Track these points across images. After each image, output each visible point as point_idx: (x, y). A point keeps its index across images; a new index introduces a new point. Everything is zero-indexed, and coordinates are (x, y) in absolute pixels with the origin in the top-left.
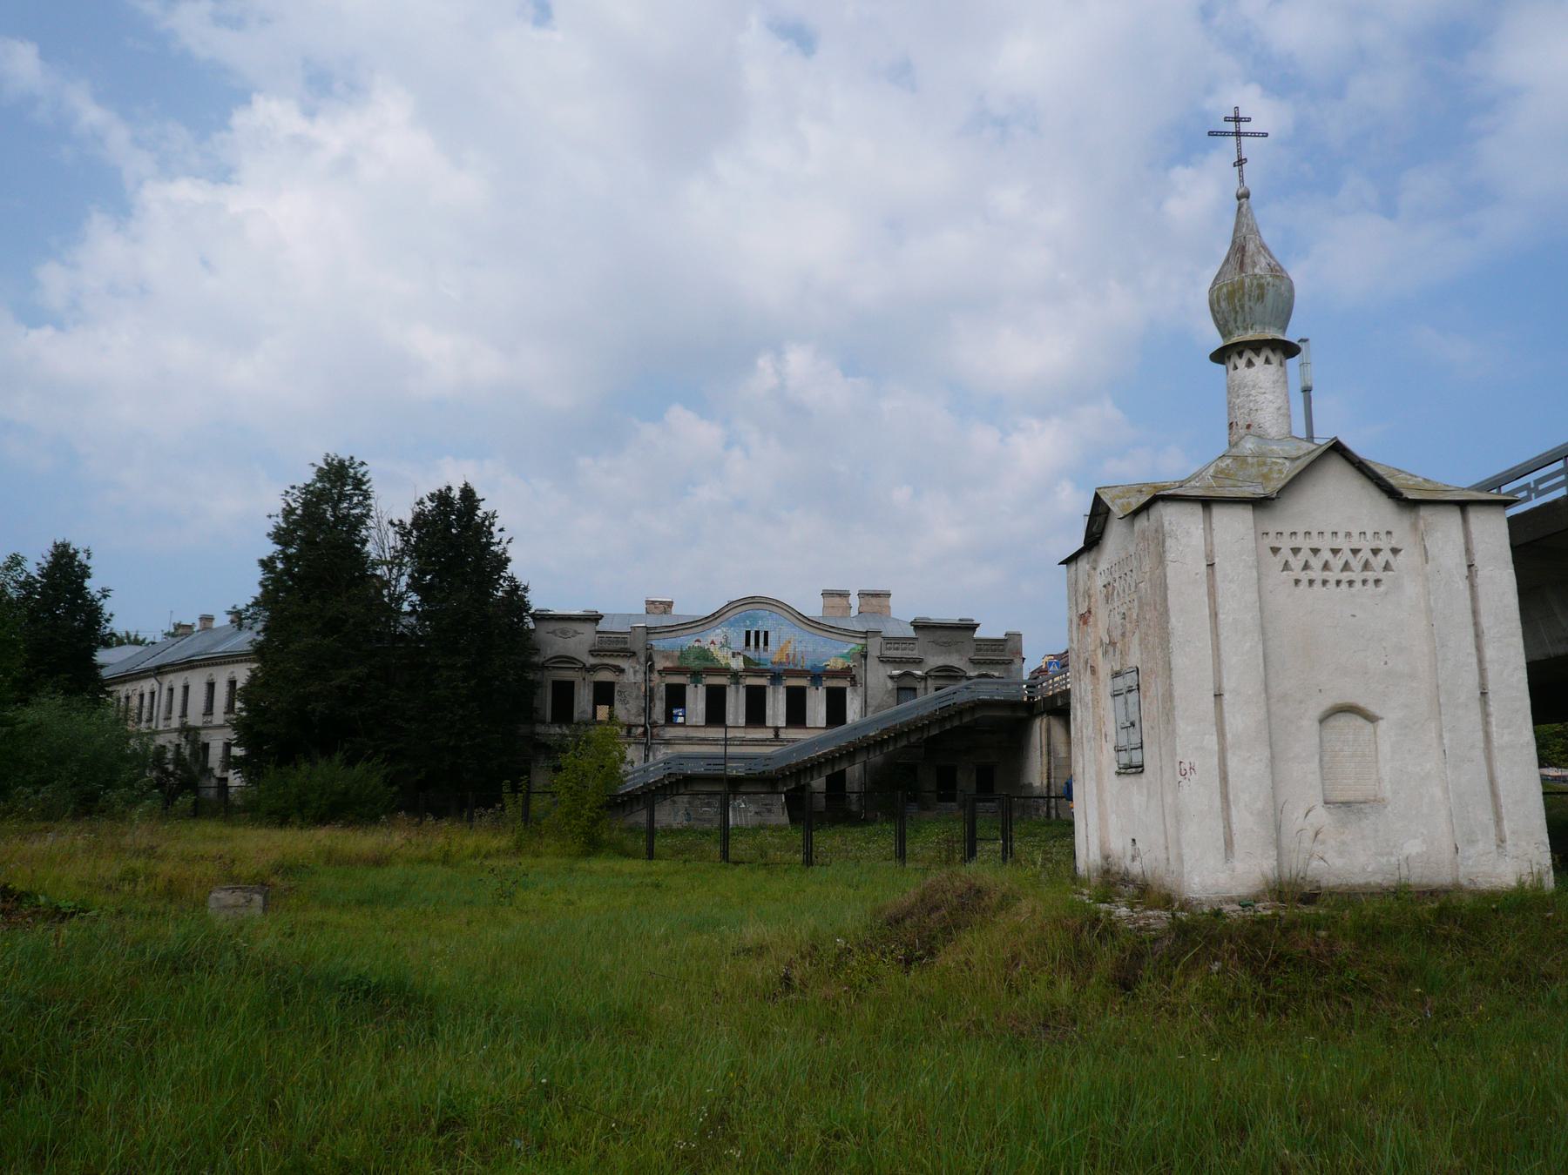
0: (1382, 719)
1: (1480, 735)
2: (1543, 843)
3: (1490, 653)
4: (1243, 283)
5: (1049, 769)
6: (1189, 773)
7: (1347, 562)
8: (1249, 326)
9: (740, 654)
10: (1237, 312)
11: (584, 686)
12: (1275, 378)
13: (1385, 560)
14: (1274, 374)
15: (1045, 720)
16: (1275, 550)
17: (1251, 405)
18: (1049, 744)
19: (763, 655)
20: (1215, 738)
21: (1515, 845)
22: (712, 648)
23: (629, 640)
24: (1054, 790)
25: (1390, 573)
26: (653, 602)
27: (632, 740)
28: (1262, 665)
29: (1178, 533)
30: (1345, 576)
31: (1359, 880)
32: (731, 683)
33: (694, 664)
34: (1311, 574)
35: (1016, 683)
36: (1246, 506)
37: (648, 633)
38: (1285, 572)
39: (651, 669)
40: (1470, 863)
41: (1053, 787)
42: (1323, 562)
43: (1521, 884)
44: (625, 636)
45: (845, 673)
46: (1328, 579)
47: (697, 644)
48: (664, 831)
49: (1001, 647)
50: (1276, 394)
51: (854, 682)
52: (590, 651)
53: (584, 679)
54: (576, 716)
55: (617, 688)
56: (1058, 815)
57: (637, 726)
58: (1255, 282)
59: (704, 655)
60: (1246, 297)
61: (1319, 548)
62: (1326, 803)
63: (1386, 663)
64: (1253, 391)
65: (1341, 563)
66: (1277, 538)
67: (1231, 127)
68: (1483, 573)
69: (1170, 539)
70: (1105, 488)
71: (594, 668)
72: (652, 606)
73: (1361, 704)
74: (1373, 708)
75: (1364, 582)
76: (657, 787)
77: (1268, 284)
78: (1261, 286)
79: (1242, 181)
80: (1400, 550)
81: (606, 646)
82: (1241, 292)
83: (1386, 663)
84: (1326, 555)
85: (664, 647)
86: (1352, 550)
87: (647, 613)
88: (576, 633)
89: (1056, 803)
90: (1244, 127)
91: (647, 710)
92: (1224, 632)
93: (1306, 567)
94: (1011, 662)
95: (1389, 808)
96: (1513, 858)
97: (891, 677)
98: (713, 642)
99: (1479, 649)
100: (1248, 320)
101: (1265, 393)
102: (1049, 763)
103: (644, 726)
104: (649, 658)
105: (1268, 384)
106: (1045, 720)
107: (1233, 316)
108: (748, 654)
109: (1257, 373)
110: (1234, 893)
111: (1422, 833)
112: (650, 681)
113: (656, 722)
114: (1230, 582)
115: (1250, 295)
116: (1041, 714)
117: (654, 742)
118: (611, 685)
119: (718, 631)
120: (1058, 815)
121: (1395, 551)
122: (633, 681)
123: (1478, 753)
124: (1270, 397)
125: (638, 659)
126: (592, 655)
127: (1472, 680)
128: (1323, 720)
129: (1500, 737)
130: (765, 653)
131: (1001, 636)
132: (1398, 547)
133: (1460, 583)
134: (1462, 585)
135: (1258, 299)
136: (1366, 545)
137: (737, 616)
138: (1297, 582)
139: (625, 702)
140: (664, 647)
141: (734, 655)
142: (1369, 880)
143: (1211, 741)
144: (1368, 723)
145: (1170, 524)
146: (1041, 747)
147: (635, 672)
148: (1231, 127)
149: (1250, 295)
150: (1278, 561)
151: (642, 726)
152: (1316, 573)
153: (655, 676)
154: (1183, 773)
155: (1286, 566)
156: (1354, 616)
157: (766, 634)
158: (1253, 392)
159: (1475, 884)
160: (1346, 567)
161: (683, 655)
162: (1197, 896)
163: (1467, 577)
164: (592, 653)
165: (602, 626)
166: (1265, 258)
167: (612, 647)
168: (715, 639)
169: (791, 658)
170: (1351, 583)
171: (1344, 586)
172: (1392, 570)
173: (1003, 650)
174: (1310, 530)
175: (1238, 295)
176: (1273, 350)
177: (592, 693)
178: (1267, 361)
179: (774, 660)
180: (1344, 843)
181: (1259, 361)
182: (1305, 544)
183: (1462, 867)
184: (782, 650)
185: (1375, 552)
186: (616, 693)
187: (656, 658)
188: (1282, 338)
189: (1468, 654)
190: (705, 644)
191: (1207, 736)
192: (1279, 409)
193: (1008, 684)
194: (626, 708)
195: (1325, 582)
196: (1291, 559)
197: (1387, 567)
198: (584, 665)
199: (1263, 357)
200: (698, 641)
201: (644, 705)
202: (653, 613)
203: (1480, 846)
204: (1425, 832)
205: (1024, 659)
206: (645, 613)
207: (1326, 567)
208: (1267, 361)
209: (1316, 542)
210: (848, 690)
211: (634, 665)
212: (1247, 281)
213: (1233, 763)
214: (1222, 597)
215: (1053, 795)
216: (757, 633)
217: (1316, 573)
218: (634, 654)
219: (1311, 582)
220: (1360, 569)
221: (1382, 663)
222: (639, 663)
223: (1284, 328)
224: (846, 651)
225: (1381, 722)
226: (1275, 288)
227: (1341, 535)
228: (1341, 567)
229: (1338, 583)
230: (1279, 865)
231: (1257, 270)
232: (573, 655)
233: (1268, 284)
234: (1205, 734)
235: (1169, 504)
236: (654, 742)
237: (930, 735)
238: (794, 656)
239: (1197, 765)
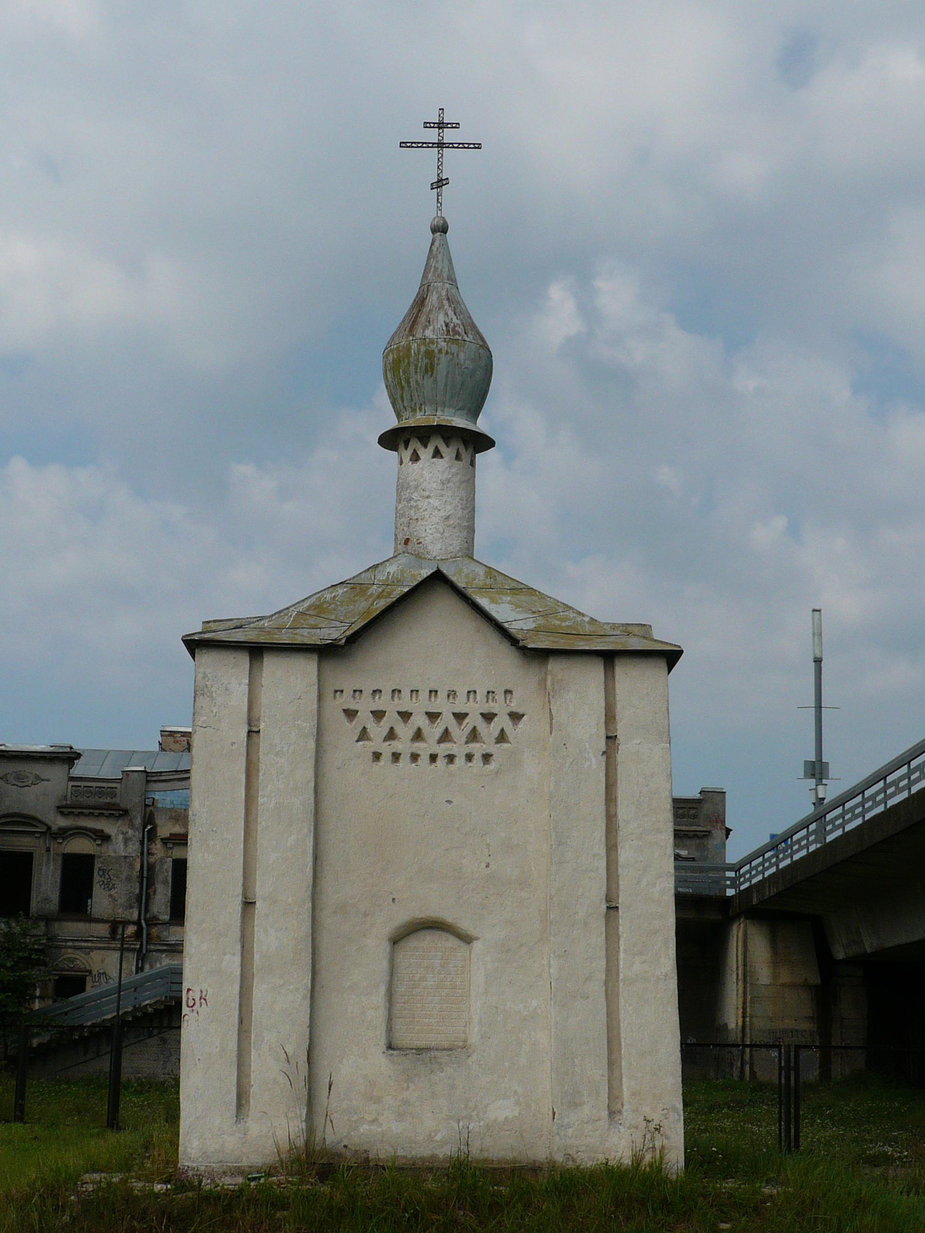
0: (477, 939)
1: (601, 963)
2: (675, 1109)
3: (625, 855)
4: (409, 349)
5: (744, 1003)
6: (198, 1004)
7: (446, 730)
8: (418, 406)
10: (402, 388)
11: (48, 860)
12: (446, 476)
13: (500, 728)
14: (444, 472)
15: (742, 925)
16: (351, 714)
17: (412, 512)
18: (745, 965)
20: (238, 959)
21: (636, 1111)
23: (118, 791)
24: (749, 1035)
25: (505, 745)
26: (172, 733)
28: (310, 864)
29: (214, 689)
31: (423, 1151)
34: (397, 746)
35: (716, 869)
36: (309, 655)
37: (148, 782)
38: (361, 743)
39: (152, 835)
40: (570, 1131)
41: (748, 1030)
42: (415, 729)
43: (637, 1160)
44: (114, 785)
46: (418, 752)
48: (141, 1084)
49: (692, 812)
50: (444, 499)
52: (58, 807)
53: (48, 850)
54: (34, 905)
55: (97, 865)
56: (753, 1073)
58: (423, 349)
60: (412, 368)
61: (410, 711)
62: (390, 1047)
63: (487, 866)
64: (416, 494)
65: (438, 731)
66: (354, 697)
67: (432, 135)
69: (202, 697)
70: (215, 621)
71: (64, 834)
72: (171, 739)
73: (448, 917)
74: (465, 925)
75: (469, 757)
76: (134, 1017)
77: (440, 351)
78: (429, 354)
79: (439, 209)
80: (523, 715)
81: (83, 800)
82: (406, 361)
83: (487, 866)
85: (172, 802)
86: (454, 714)
87: (163, 750)
88: (39, 779)
89: (751, 1056)
90: (449, 136)
91: (143, 899)
92: (263, 821)
93: (391, 735)
94: (707, 835)
95: (474, 1057)
96: (629, 1128)
99: (611, 848)
100: (415, 398)
101: (428, 497)
102: (745, 993)
104: (149, 819)
105: (434, 485)
106: (742, 925)
107: (399, 392)
109: (422, 469)
110: (245, 1163)
111: (515, 1091)
112: (149, 854)
113: (155, 918)
114: (277, 754)
115: (416, 366)
116: (737, 916)
117: (152, 947)
118: (88, 860)
120: (753, 1073)
121: (516, 717)
122: (123, 854)
123: (597, 988)
124: (435, 502)
125: (131, 820)
126: (62, 813)
127: (596, 891)
128: (397, 939)
129: (629, 967)
131: (694, 794)
132: (520, 711)
133: (593, 760)
134: (596, 763)
135: (426, 371)
136: (474, 709)
138: (377, 756)
139: (108, 886)
140: (172, 802)
142: (436, 1152)
143: (233, 963)
144: (462, 944)
145: (204, 677)
146: (737, 968)
147: (126, 841)
148: (432, 135)
149: (416, 366)
150: (353, 729)
151: (134, 923)
152: (403, 745)
153: (158, 848)
154: (191, 1004)
155: (363, 735)
156: (449, 802)
158: (415, 496)
159: (574, 1160)
160: (446, 736)
162: (195, 1165)
163: (604, 753)
164: (63, 810)
165: (78, 770)
166: (446, 314)
167: (93, 801)
170: (451, 758)
171: (441, 762)
172: (509, 742)
173: (695, 816)
174: (398, 687)
175: (403, 365)
176: (447, 442)
177: (59, 873)
178: (458, 457)
180: (406, 1102)
181: (425, 453)
182: (391, 707)
183: (557, 1138)
185: (488, 717)
186: (96, 873)
187: (159, 821)
188: (471, 427)
189: (595, 855)
191: (228, 957)
192: (448, 518)
193: (701, 870)
194: (111, 896)
195: (415, 757)
196: (371, 725)
197: (502, 737)
198: (49, 828)
199: (430, 449)
201: (137, 891)
202: (171, 750)
203: (586, 1111)
204: (520, 1090)
205: (728, 831)
206: (156, 748)
208: (437, 454)
209: (405, 704)
211: (125, 829)
212: (414, 346)
213: (260, 993)
214: (264, 774)
215: (748, 1043)
217: (403, 745)
218: (125, 812)
219: (396, 757)
220: (464, 739)
221: (483, 865)
222: (132, 826)
223: (475, 411)
225: (475, 942)
226: (450, 356)
227: (442, 695)
228: (437, 736)
229: (433, 758)
230: (310, 1130)
231: (429, 333)
232: (32, 813)
233: (440, 351)
234: (225, 954)
235: (204, 651)
236: (152, 947)
239: (210, 992)
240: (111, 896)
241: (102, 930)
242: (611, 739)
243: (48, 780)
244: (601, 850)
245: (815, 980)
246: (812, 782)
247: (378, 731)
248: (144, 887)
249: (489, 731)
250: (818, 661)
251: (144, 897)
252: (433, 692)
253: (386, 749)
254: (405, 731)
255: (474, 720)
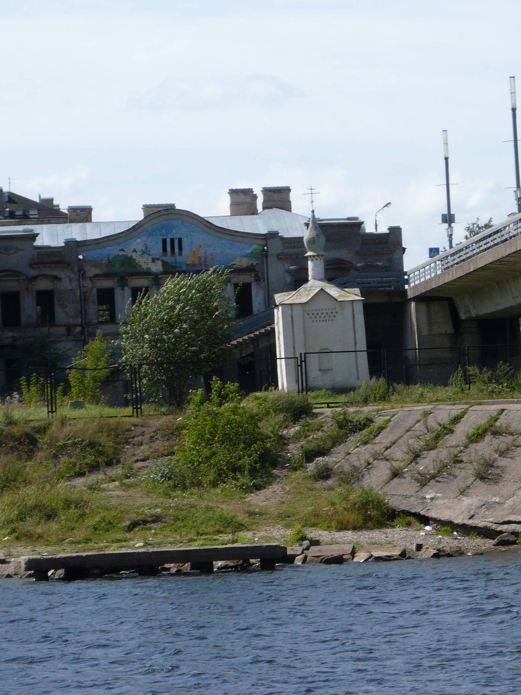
3: (357, 335)
9: (158, 259)
16: (308, 314)
19: (179, 259)
22: (134, 256)
27: (71, 337)
30: (325, 319)
32: (153, 285)
33: (118, 269)
37: (79, 246)
45: (250, 269)
47: (121, 253)
51: (258, 279)
53: (27, 289)
54: (24, 319)
55: (56, 296)
57: (75, 326)
59: (128, 261)
62: (320, 370)
65: (323, 316)
68: (356, 316)
71: (35, 278)
84: (320, 314)
88: (17, 249)
90: (313, 191)
93: (315, 317)
97: (289, 272)
98: (135, 251)
103: (81, 325)
108: (165, 259)
119: (139, 241)
122: (70, 288)
126: (33, 268)
127: (353, 342)
130: (181, 257)
137: (154, 227)
138: (313, 321)
140: (93, 257)
141: (154, 260)
147: (71, 281)
151: (79, 325)
153: (88, 283)
155: (311, 318)
157: (180, 240)
160: (325, 317)
161: (110, 263)
164: (32, 265)
168: (136, 247)
169: (203, 260)
170: (326, 321)
179: (188, 263)
184: (194, 253)
190: (128, 252)
194: (65, 312)
200: (122, 250)
201: (79, 308)
207: (332, 313)
208: (317, 259)
210: (253, 285)
211: (69, 274)
216: (172, 240)
217: (318, 319)
224: (249, 251)
237: (421, 281)
238: (205, 258)
240: (65, 312)
241: (62, 330)
242: (353, 315)
243: (23, 250)
244: (353, 334)
245: (450, 329)
246: (446, 225)
247: (313, 317)
248: (83, 306)
249: (332, 316)
250: (446, 159)
251: (83, 311)
252: (322, 309)
253: (315, 320)
254: (318, 317)
255: (330, 314)
